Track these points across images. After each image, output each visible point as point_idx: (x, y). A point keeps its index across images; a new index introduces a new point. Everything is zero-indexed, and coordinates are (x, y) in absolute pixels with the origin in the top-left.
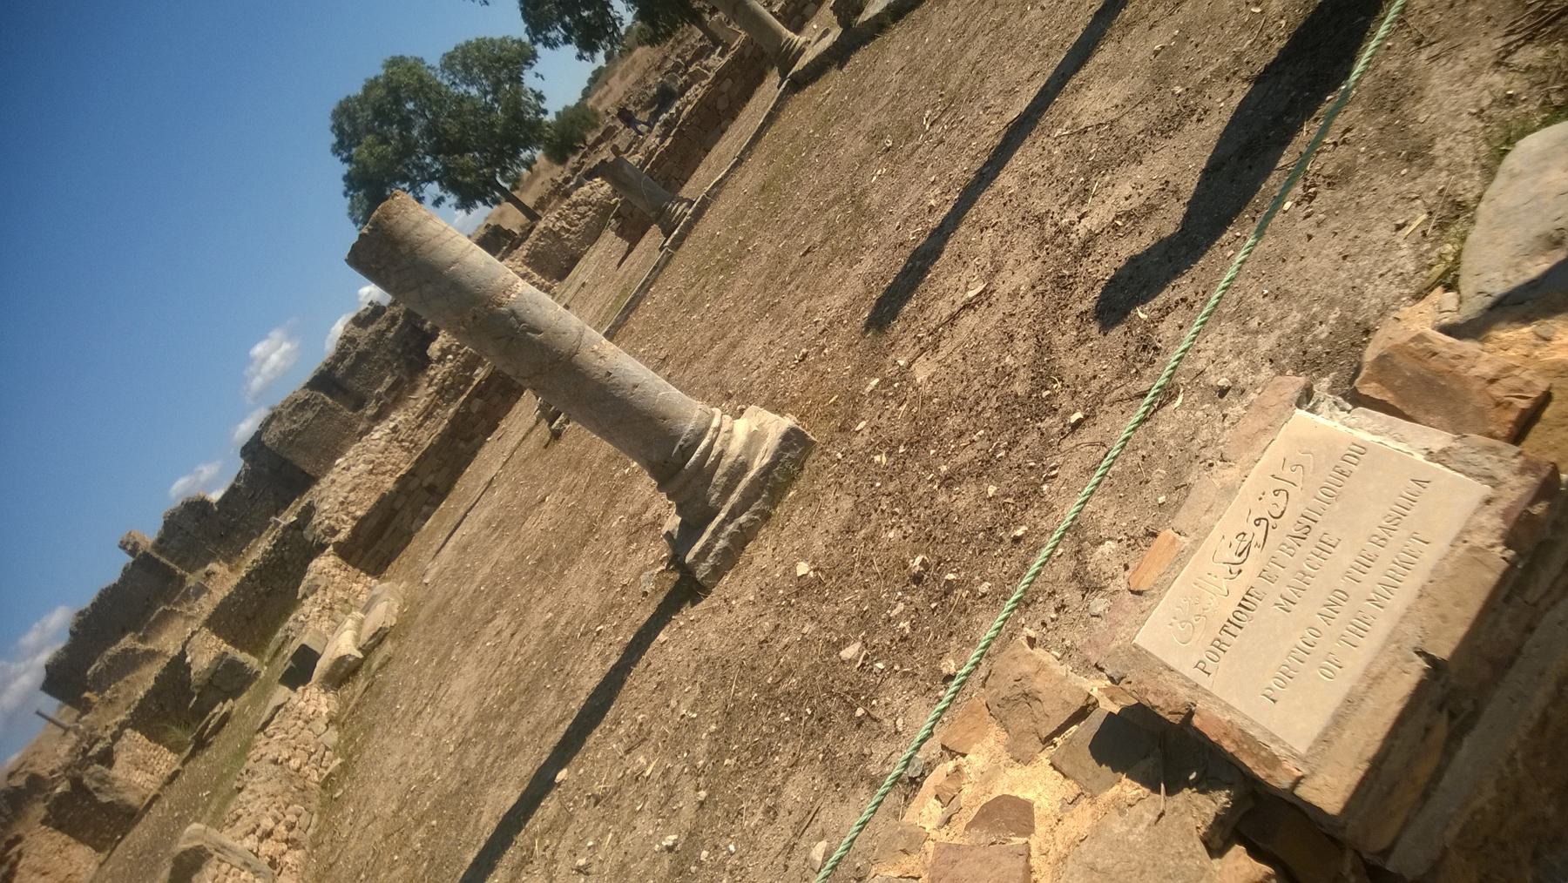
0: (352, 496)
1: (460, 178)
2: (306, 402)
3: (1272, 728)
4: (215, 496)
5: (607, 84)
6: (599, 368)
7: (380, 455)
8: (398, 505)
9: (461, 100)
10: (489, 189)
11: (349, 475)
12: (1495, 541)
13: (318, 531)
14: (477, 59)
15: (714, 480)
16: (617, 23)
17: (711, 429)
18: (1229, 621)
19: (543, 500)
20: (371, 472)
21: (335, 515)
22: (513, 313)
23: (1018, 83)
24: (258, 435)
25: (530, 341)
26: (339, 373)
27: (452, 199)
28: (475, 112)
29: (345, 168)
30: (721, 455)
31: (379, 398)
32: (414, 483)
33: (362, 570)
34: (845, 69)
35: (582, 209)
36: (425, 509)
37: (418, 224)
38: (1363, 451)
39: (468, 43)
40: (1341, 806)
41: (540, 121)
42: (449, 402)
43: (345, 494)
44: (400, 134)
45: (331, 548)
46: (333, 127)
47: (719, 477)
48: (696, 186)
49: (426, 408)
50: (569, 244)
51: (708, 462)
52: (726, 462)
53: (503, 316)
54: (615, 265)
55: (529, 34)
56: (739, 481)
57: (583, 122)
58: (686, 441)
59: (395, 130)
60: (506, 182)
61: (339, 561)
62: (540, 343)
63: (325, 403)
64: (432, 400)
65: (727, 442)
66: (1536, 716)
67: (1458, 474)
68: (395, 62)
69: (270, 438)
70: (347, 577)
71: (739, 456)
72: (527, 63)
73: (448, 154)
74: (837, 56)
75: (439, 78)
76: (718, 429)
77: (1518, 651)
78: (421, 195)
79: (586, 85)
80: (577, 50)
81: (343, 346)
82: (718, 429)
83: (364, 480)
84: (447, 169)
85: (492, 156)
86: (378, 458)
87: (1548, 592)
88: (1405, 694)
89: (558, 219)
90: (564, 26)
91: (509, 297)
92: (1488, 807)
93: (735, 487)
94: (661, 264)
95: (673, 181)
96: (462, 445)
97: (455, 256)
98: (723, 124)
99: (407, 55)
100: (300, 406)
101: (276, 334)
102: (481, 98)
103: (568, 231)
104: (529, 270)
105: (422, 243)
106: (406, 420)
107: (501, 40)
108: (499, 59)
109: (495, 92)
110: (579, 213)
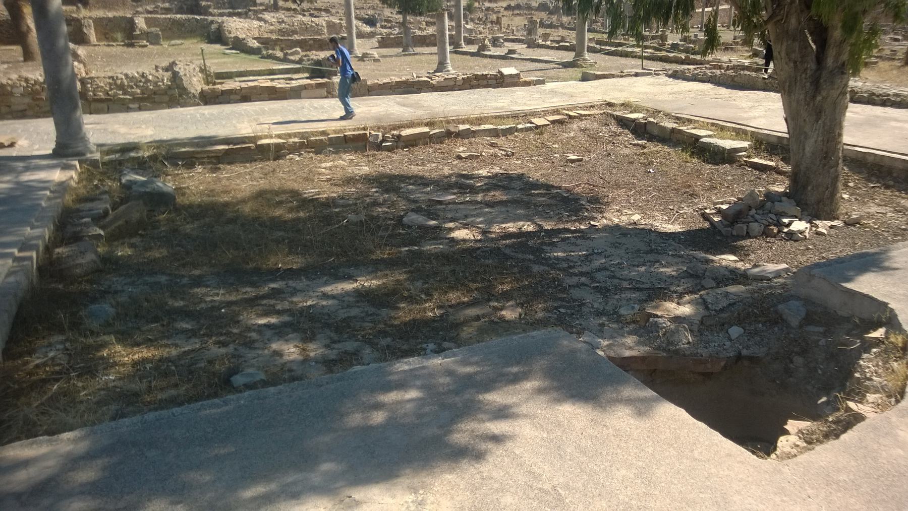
0: (240, 30)
20: (248, 29)
31: (157, 7)
42: (279, 35)
48: (418, 50)
49: (272, 30)
74: (472, 54)
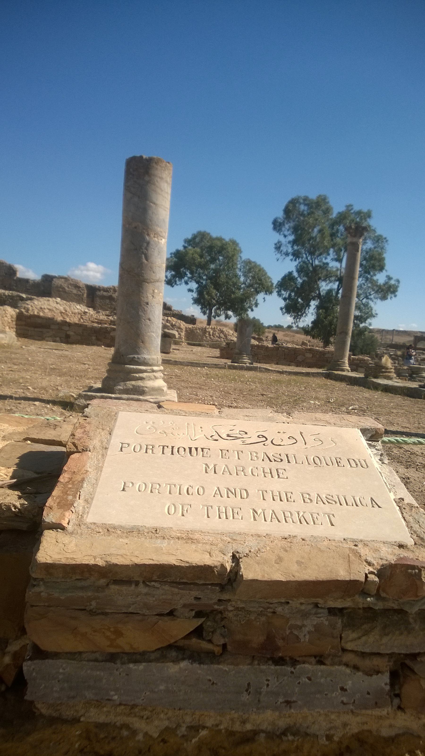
1: (205, 293)
2: (79, 287)
3: (98, 496)
4: (19, 275)
5: (278, 331)
6: (147, 297)
7: (71, 313)
8: (53, 327)
9: (236, 276)
10: (208, 307)
11: (55, 305)
12: (375, 563)
13: (24, 305)
14: (255, 272)
15: (128, 382)
16: (304, 314)
17: (151, 367)
18: (173, 447)
19: (85, 364)
20: (61, 313)
21: (34, 308)
22: (148, 243)
23: (398, 424)
24: (55, 277)
25: (140, 259)
26: (98, 293)
27: (195, 295)
28: (234, 284)
29: (181, 248)
30: (142, 379)
32: (66, 328)
33: (16, 328)
34: (348, 386)
35: (222, 335)
36: (58, 339)
37: (162, 178)
38: (365, 466)
39: (259, 266)
40: (49, 561)
41: (246, 310)
43: (46, 307)
44: (208, 261)
45: (18, 311)
46: (194, 234)
47: (130, 384)
49: (102, 320)
50: (205, 338)
51: (135, 375)
52: (140, 383)
53: (144, 239)
54: (207, 356)
55: (277, 283)
56: (134, 395)
57: (258, 330)
58: (138, 358)
59: (208, 258)
60: (215, 312)
61: (15, 316)
62: (142, 263)
63: (83, 295)
64: (107, 321)
65: (150, 379)
66: (249, 727)
67: (403, 520)
68: (234, 243)
69: (56, 282)
70: (9, 323)
71: (146, 387)
72: (266, 292)
73: (211, 283)
75: (238, 263)
76: (153, 371)
77: (294, 662)
78: (189, 282)
79: (273, 325)
80: (283, 306)
81: (110, 289)
82: (153, 371)
83: (56, 312)
84: (205, 286)
85: (221, 300)
86: (69, 312)
87: (363, 655)
88: (190, 560)
89: (212, 328)
90: (290, 295)
91: (154, 237)
92: (140, 737)
93: (130, 394)
94: (219, 366)
95: (256, 357)
96: (94, 338)
97: (158, 202)
98: (292, 363)
99: (240, 245)
100: (77, 286)
101: (101, 268)
102: (241, 283)
103: (210, 335)
104: (184, 329)
105: (154, 184)
106: (92, 315)
107: (268, 277)
108: (260, 280)
109: (248, 287)
110: (219, 335)
